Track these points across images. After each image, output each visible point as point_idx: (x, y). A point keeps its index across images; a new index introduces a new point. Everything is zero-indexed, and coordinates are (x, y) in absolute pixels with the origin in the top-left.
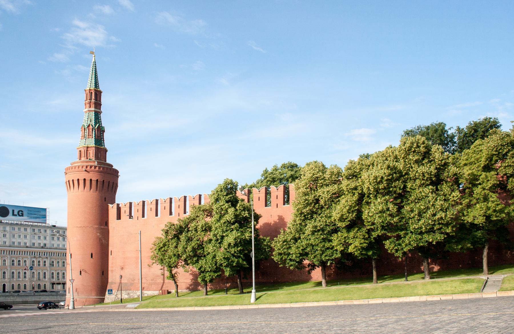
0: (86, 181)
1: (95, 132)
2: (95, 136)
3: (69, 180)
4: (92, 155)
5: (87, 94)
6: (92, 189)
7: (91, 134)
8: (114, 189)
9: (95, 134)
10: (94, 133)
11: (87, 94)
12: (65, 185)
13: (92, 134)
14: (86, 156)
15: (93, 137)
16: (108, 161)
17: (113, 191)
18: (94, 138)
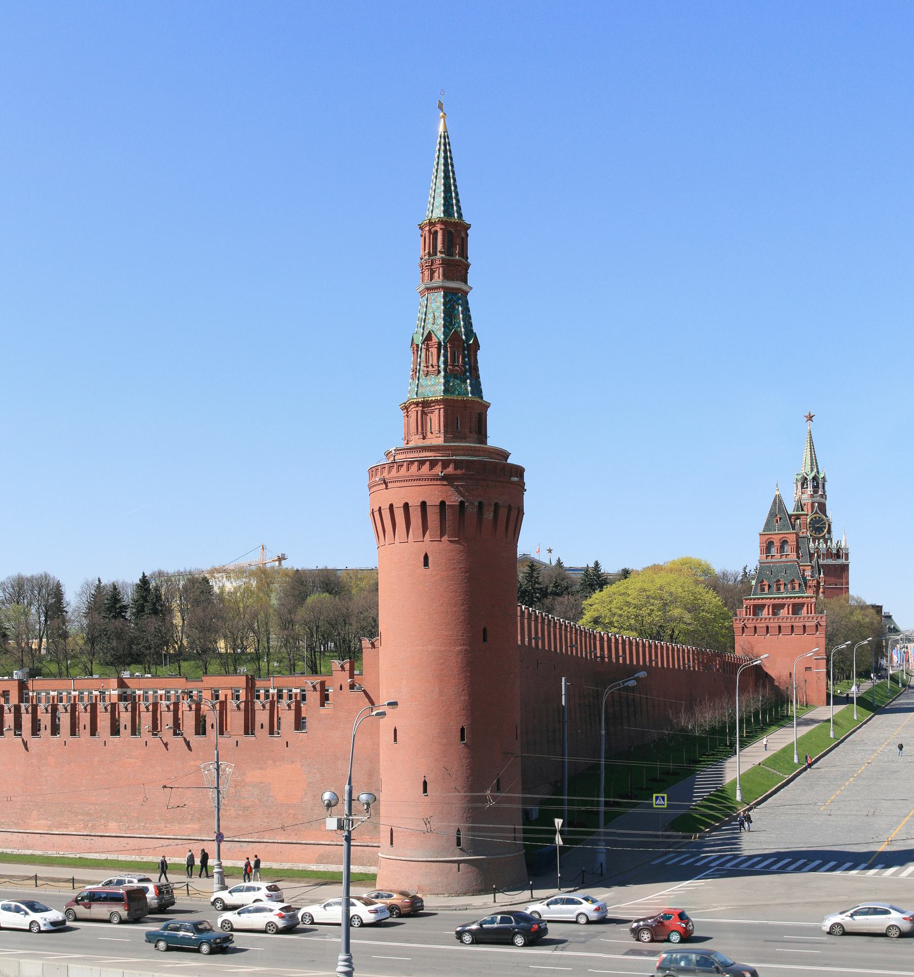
0: (428, 508)
1: (445, 356)
2: (445, 370)
3: (380, 508)
4: (437, 428)
5: (425, 238)
6: (428, 533)
7: (435, 363)
8: (511, 529)
9: (445, 363)
10: (442, 359)
11: (425, 238)
12: (370, 520)
13: (438, 362)
14: (422, 430)
15: (439, 372)
16: (494, 440)
17: (510, 533)
18: (442, 373)
